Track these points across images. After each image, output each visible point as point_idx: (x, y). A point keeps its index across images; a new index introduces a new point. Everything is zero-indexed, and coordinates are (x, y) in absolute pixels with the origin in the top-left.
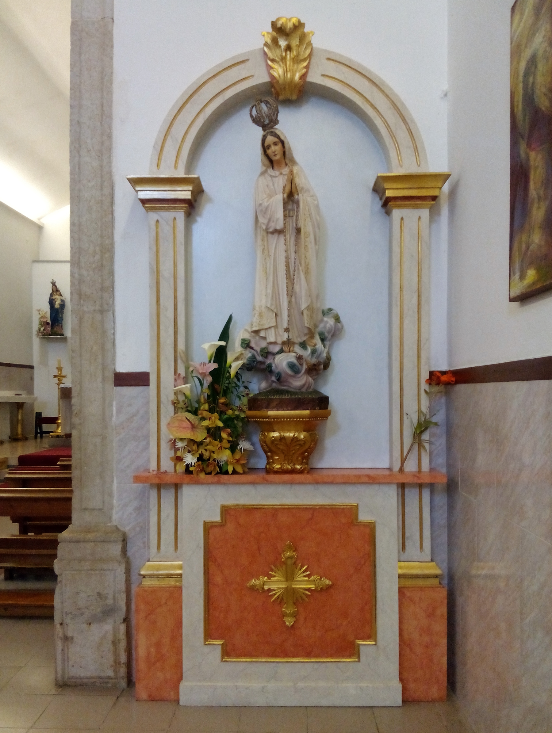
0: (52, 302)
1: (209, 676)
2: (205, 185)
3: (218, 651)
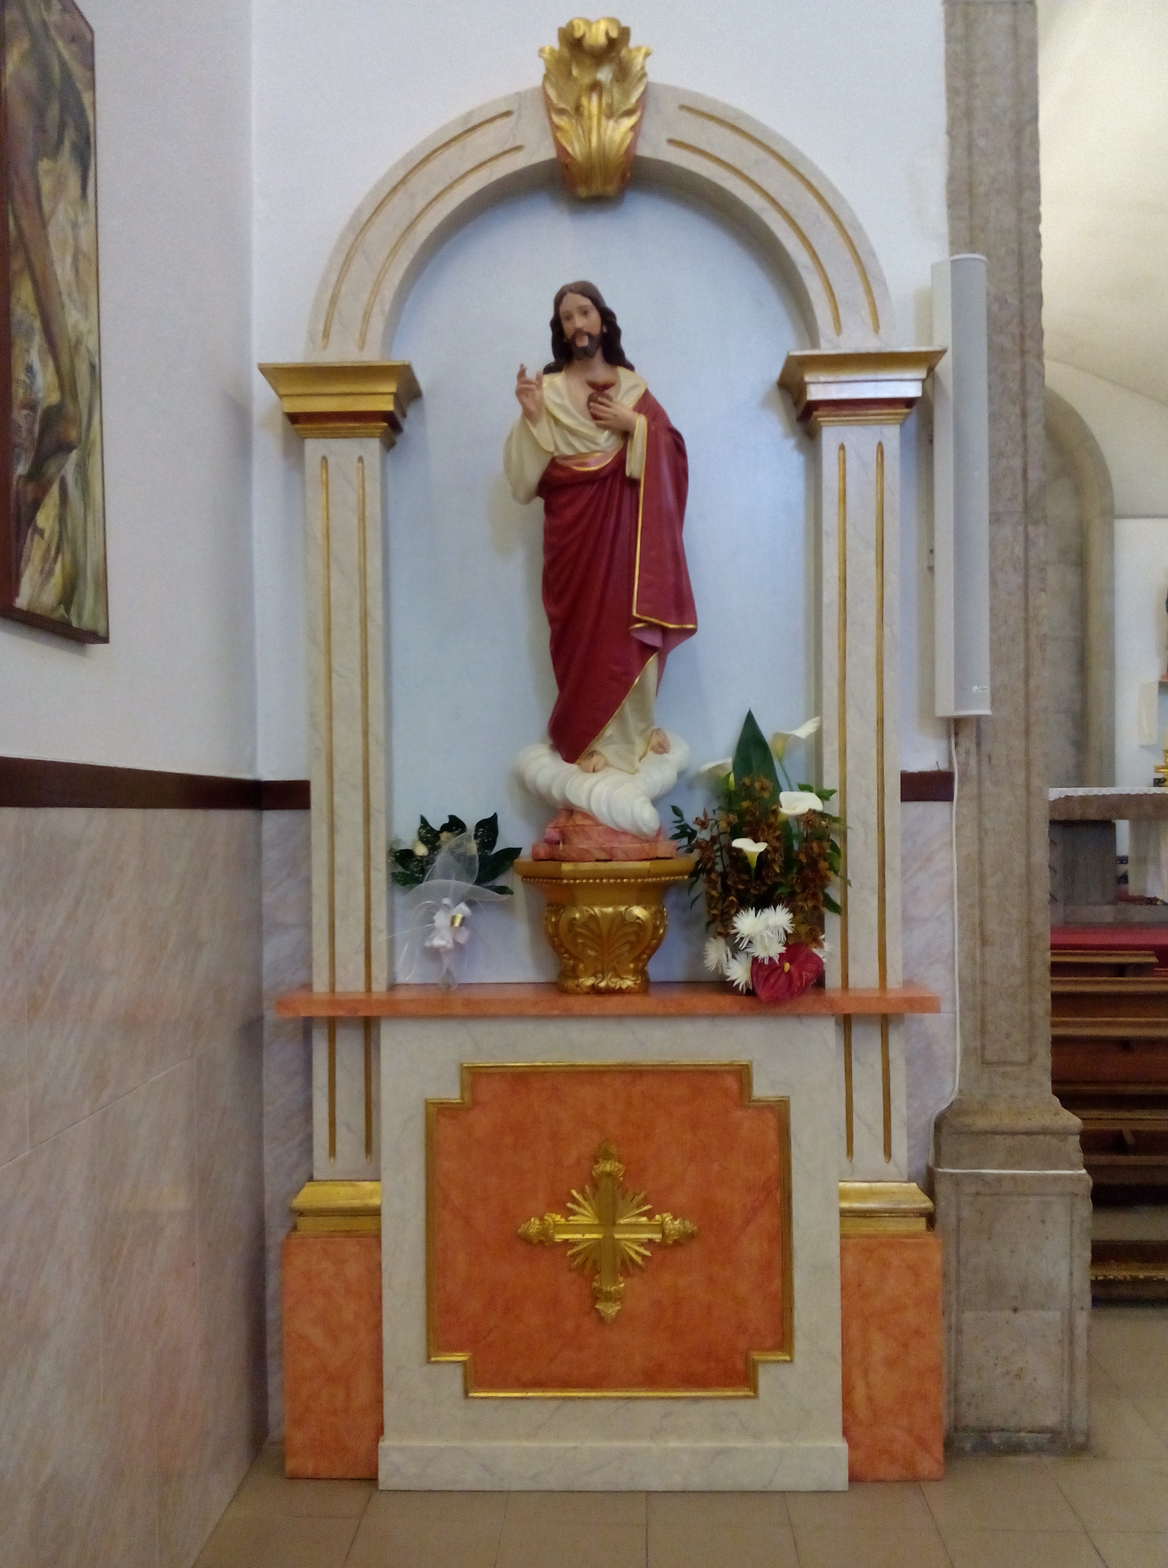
1: (442, 1431)
2: (423, 379)
3: (454, 1380)
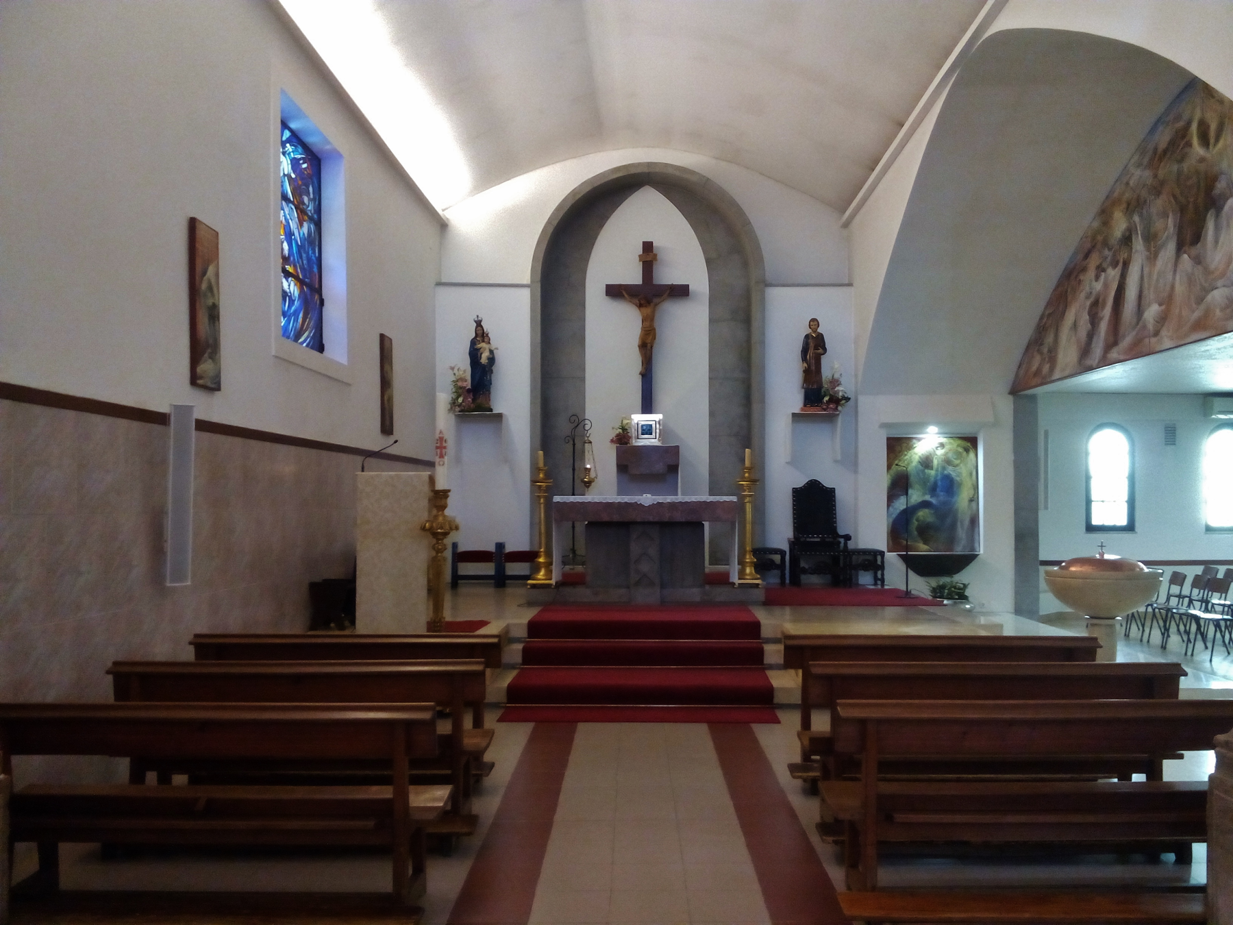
0: (474, 354)
